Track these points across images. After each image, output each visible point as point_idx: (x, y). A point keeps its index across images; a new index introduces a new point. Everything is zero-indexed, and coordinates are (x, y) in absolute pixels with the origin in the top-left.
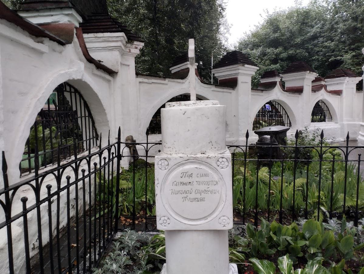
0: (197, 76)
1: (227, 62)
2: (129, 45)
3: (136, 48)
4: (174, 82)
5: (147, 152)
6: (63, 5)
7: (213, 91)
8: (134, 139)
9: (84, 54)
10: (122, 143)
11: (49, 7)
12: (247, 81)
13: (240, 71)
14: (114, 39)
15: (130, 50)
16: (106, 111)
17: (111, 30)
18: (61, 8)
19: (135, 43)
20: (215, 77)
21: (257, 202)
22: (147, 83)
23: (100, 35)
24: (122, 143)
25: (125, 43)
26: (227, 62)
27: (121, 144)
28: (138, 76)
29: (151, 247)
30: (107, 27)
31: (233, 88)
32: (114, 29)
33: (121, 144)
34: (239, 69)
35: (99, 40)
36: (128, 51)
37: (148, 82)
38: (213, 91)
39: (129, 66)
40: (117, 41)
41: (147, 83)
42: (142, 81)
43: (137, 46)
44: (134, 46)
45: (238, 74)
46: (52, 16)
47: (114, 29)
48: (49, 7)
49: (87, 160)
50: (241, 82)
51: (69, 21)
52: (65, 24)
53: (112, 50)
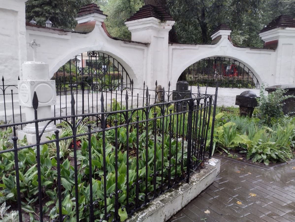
0: (230, 41)
1: (270, 26)
2: (163, 24)
3: (169, 25)
4: (205, 47)
5: (4, 91)
6: (92, 12)
7: (247, 53)
8: (162, 88)
9: (108, 36)
10: (217, 90)
11: (87, 13)
12: (292, 43)
13: (280, 34)
14: (148, 22)
15: (164, 27)
16: (132, 68)
17: (146, 16)
18: (90, 13)
19: (168, 22)
20: (262, 40)
21: (27, 123)
22: (179, 49)
23: (140, 20)
24: (217, 90)
25: (158, 23)
26: (270, 26)
27: (215, 88)
28: (173, 45)
29: (197, 160)
30: (146, 14)
31: (274, 49)
32: (149, 16)
33: (215, 88)
34: (279, 33)
35: (140, 24)
36: (163, 28)
37: (180, 48)
38: (247, 53)
39: (164, 38)
40: (150, 23)
41: (179, 49)
42: (175, 48)
43: (169, 24)
44: (167, 24)
45: (278, 37)
46: (88, 18)
47: (149, 16)
48: (87, 13)
49: (209, 98)
50: (283, 44)
51: (94, 20)
52: (93, 21)
53: (147, 29)
